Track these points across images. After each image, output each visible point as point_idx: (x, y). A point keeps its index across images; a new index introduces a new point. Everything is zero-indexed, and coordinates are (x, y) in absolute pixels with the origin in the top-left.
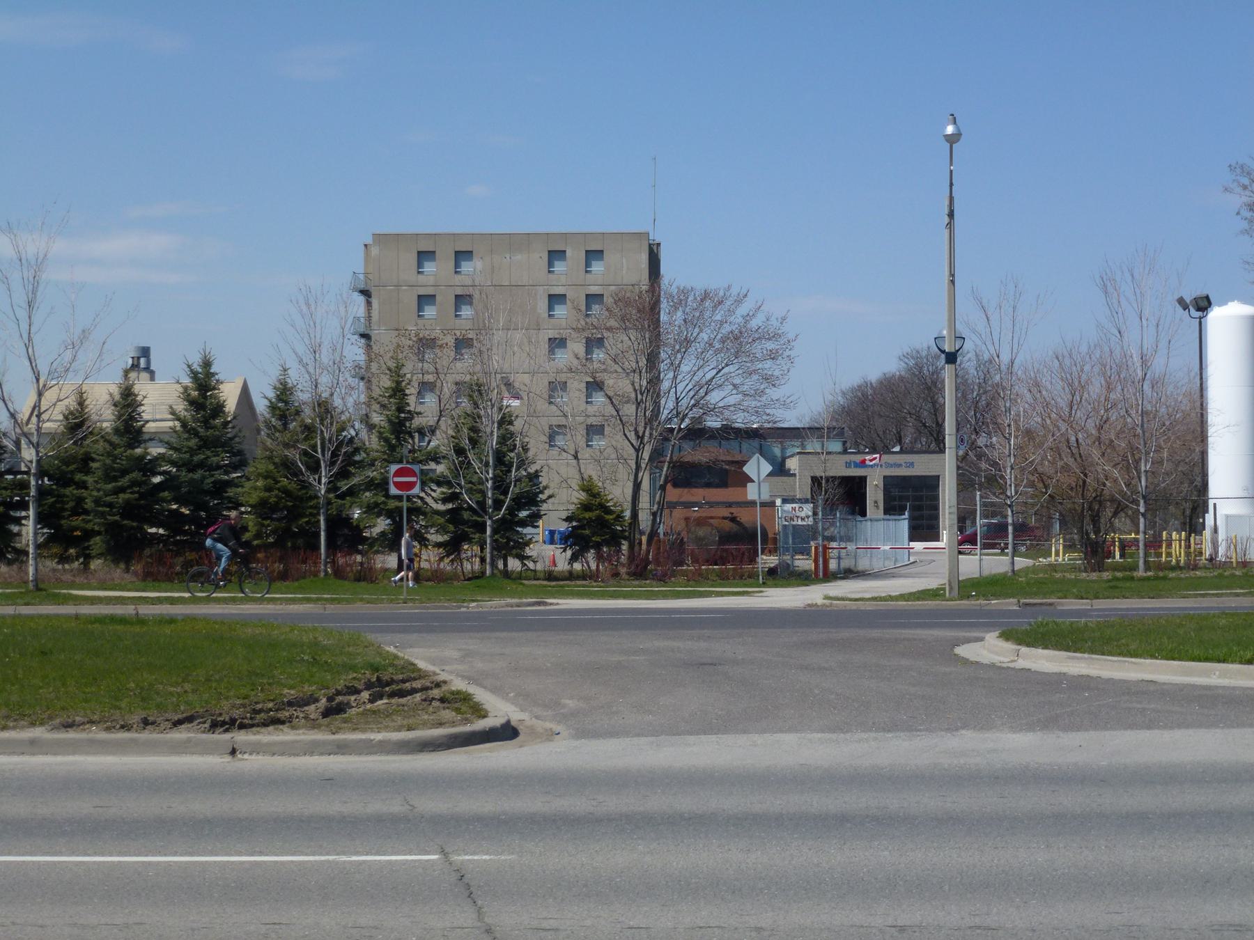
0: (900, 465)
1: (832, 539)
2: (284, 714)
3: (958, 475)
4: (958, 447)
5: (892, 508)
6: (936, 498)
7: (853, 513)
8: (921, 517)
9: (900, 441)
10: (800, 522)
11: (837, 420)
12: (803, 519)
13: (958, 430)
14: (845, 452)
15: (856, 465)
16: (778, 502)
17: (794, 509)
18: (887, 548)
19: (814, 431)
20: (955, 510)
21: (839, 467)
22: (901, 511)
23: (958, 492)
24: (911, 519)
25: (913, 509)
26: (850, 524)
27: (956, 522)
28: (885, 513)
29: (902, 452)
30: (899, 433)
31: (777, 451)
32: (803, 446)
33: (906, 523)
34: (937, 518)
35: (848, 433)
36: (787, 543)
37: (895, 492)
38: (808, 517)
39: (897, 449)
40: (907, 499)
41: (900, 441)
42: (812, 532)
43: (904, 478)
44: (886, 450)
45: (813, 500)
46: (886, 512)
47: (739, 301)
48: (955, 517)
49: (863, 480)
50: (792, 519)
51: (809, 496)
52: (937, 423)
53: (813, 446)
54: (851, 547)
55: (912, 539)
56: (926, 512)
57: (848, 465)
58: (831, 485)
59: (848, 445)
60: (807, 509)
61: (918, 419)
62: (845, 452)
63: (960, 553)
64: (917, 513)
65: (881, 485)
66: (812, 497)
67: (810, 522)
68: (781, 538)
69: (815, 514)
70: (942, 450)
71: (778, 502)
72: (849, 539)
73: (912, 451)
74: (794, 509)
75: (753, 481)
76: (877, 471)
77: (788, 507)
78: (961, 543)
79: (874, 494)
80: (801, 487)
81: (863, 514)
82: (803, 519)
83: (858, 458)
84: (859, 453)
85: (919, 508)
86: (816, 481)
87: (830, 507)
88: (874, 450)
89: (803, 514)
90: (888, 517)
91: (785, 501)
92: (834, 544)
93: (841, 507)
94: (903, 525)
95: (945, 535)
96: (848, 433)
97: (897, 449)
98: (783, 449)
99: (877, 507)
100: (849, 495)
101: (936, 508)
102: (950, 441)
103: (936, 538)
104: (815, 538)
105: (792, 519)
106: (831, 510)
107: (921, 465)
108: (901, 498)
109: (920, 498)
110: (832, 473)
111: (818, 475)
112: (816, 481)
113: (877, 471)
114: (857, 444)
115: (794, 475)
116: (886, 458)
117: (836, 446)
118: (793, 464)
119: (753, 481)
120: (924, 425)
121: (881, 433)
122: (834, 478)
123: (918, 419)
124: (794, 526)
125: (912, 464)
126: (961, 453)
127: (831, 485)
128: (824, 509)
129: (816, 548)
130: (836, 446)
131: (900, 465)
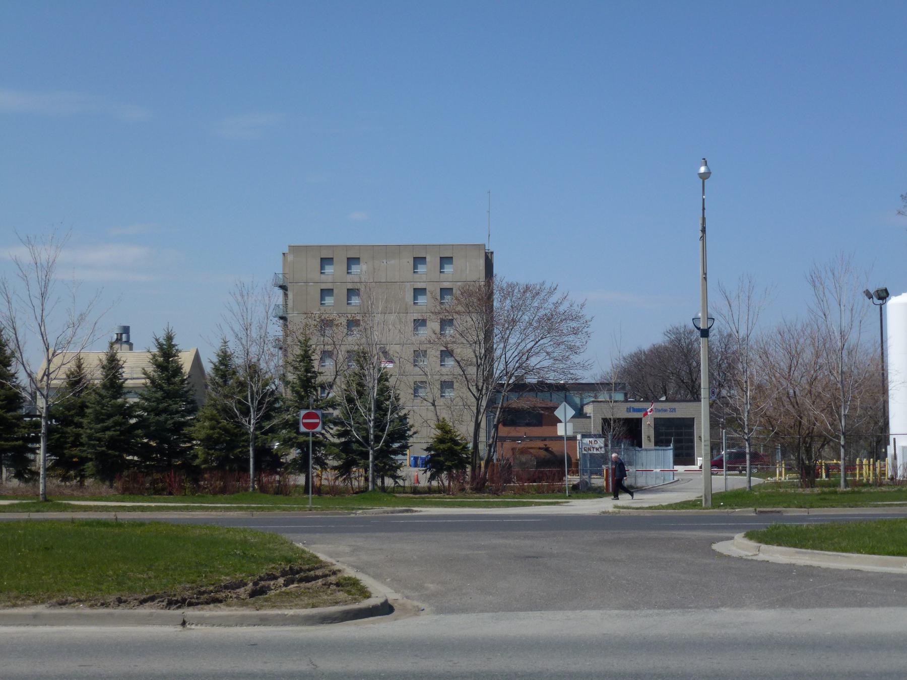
0: (665, 411)
7: (633, 445)
10: (595, 452)
12: (597, 449)
14: (626, 401)
16: (579, 437)
17: (591, 442)
18: (658, 470)
19: (605, 386)
20: (709, 443)
22: (667, 443)
24: (675, 449)
25: (676, 441)
28: (656, 445)
29: (667, 400)
30: (664, 387)
31: (577, 400)
32: (596, 397)
35: (628, 387)
37: (663, 430)
39: (663, 398)
40: (671, 434)
41: (665, 393)
44: (656, 400)
45: (603, 435)
49: (639, 421)
53: (603, 396)
55: (676, 463)
57: (628, 410)
60: (601, 442)
61: (678, 376)
64: (679, 445)
65: (653, 425)
67: (603, 451)
69: (606, 445)
71: (579, 437)
73: (674, 401)
74: (591, 442)
76: (650, 415)
77: (586, 440)
79: (647, 431)
80: (595, 426)
81: (640, 446)
82: (597, 449)
86: (606, 421)
87: (617, 441)
89: (597, 446)
91: (584, 436)
95: (700, 461)
97: (663, 398)
98: (582, 400)
99: (650, 440)
102: (704, 393)
103: (692, 462)
104: (606, 464)
106: (618, 443)
107: (681, 410)
112: (606, 421)
113: (650, 415)
114: (634, 396)
115: (590, 417)
117: (620, 396)
118: (588, 409)
120: (682, 381)
121: (652, 388)
122: (619, 419)
124: (591, 455)
127: (617, 424)
128: (612, 442)
129: (607, 471)
130: (620, 396)
131: (665, 411)
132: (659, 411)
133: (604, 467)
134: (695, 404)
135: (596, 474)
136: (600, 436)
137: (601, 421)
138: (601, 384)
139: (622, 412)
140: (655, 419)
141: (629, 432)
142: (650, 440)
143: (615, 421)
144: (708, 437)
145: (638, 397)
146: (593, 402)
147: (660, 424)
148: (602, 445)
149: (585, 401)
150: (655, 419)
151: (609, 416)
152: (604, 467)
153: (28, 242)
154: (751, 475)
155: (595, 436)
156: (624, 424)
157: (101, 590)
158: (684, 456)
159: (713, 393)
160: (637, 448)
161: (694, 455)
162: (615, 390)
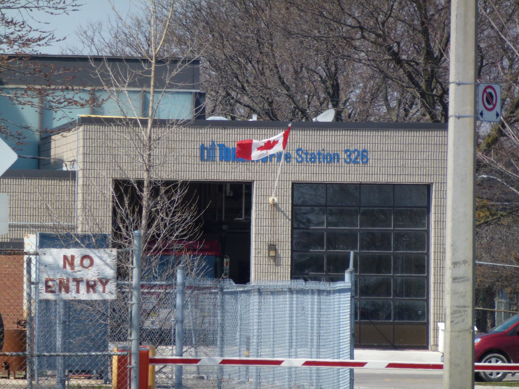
0: (333, 158)
1: (163, 337)
2: (445, 35)
3: (478, 185)
4: (478, 116)
5: (312, 261)
6: (422, 241)
7: (216, 273)
8: (382, 288)
9: (334, 97)
10: (83, 295)
11: (181, 41)
12: (91, 287)
13: (479, 73)
14: (199, 120)
15: (226, 155)
16: (31, 242)
17: (69, 261)
18: (299, 362)
19: (124, 66)
20: (467, 270)
21: (185, 159)
22: (334, 269)
23: (478, 227)
24: (360, 290)
25: (365, 265)
26: (207, 301)
27: (468, 300)
28: (294, 275)
29: (339, 123)
30: (333, 77)
31: (30, 115)
32: (95, 103)
33: (346, 300)
34: (421, 289)
35: (207, 74)
36: (49, 346)
37: (321, 224)
38: (104, 282)
39: (328, 116)
40: (350, 240)
41: (334, 97)
42: (113, 320)
43: (343, 189)
44: (302, 119)
45: (118, 239)
46: (298, 270)
47: (25, 138)
48: (467, 289)
49: (239, 194)
50: (64, 286)
51: (108, 230)
52: (429, 54)
53: (120, 102)
54: (210, 358)
55: (360, 340)
56: (396, 276)
57: (206, 153)
58: (163, 201)
59: (208, 103)
60: (104, 262)
61: (382, 39)
62: (199, 120)
63: (478, 378)
64: (373, 278)
65: (287, 208)
66: (117, 232)
67: (109, 293)
68: (35, 333)
69: (122, 274)
70: (439, 122)
71: (31, 242)
72: (205, 338)
73: (364, 124)
74: (69, 261)
75: (442, 330)
76: (275, 170)
77: (55, 255)
78: (480, 354)
79: (269, 227)
80: (89, 206)
81: (242, 275)
82: (91, 287)
83: (232, 138)
84: (233, 123)
85: (378, 264)
86: (125, 191)
87: (161, 254)
88: (271, 119)
89: (91, 275)
90: (300, 284)
91: (47, 240)
92: (167, 352)
93: (186, 257)
94: (337, 305)
95: (441, 333)
96: (207, 74)
97: (328, 116)
98: (45, 111)
99: (276, 259)
100: (212, 226)
101: (421, 265)
102: (459, 100)
103: (422, 343)
104: (120, 336)
105: (64, 286)
106: (163, 265)
107: (386, 158)
108: (333, 240)
109: (382, 241)
110: (164, 173)
111: (132, 176)
112: (125, 191)
113: (275, 170)
114: (228, 103)
115: (72, 176)
116: (298, 137)
117: (177, 106)
118: (67, 148)
119: (442, 330)
120: (396, 57)
121: (288, 78)
122: (171, 185)
123: (382, 39)
124: (68, 304)
125: (362, 156)
126: (486, 129)
127: (163, 201)
128: (144, 261)
129: (123, 361)
130: (177, 106)
131: (333, 158)
132: (313, 158)
133: (113, 348)
134: (433, 136)
135: (87, 373)
136: (101, 242)
137: (110, 191)
138: (112, 60)
139: (184, 159)
140: (296, 186)
141: (212, 226)
142: (276, 259)
143: (155, 192)
144: (466, 251)
145: (241, 111)
146: (85, 121)
147: (307, 200)
148: (110, 273)
149: (59, 118)
150: (296, 186)
151: (135, 172)
152: (113, 348)
153: (40, 85)
154: (505, 312)
155: (86, 241)
156: (186, 199)
157: (352, 91)
158: (390, 316)
159: (490, 99)
160: (230, 285)
161: (426, 313)
162: (160, 84)
